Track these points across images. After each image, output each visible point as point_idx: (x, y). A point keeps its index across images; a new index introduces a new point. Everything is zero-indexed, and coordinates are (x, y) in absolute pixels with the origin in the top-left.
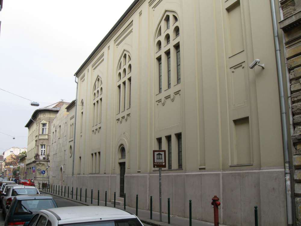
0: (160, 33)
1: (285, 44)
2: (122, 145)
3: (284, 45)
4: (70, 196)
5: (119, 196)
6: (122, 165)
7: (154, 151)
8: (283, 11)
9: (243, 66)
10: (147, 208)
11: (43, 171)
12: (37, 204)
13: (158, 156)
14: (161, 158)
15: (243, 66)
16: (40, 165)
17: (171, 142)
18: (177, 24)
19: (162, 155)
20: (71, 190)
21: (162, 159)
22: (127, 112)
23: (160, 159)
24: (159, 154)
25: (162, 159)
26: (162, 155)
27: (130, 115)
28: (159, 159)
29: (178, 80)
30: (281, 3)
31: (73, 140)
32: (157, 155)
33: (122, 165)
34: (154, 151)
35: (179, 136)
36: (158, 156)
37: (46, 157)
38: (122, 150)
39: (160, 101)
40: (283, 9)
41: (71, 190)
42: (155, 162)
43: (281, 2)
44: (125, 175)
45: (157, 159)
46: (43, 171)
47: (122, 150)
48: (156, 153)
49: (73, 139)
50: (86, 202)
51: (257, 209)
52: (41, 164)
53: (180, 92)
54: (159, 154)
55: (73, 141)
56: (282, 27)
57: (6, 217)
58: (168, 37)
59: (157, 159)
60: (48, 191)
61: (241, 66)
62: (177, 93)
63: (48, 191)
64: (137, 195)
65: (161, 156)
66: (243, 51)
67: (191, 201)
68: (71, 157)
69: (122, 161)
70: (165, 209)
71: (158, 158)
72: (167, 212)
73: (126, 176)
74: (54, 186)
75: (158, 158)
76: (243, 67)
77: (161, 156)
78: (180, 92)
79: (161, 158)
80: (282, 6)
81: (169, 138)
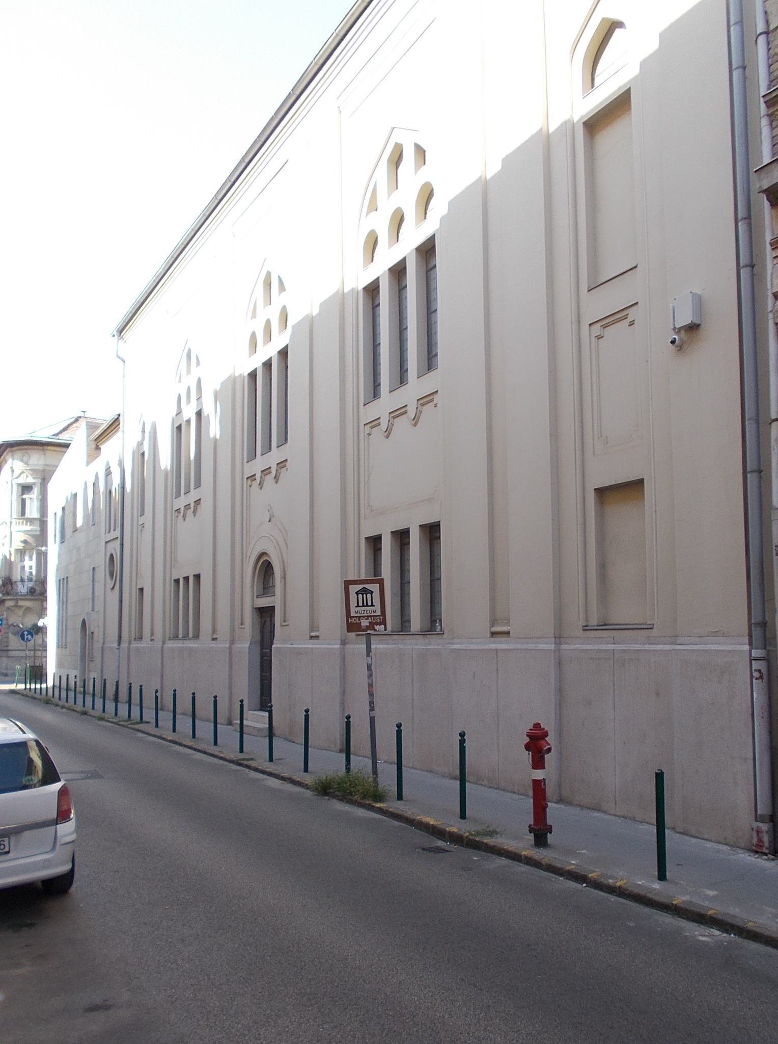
0: (373, 206)
1: (771, 244)
2: (263, 554)
3: (768, 247)
4: (110, 706)
5: (259, 707)
6: (265, 614)
7: (347, 584)
8: (772, 129)
9: (630, 319)
10: (338, 746)
11: (26, 633)
12: (73, 828)
13: (360, 596)
14: (370, 604)
15: (630, 319)
16: (20, 613)
17: (409, 548)
18: (426, 174)
19: (372, 593)
20: (184, 704)
21: (372, 605)
22: (275, 456)
23: (367, 605)
24: (364, 591)
25: (372, 605)
26: (372, 593)
27: (288, 464)
28: (363, 606)
29: (430, 360)
30: (765, 102)
31: (117, 538)
32: (357, 593)
33: (265, 614)
34: (347, 584)
35: (432, 531)
36: (360, 596)
37: (37, 588)
38: (265, 570)
39: (377, 422)
40: (775, 124)
41: (184, 704)
42: (353, 614)
43: (768, 98)
44: (273, 646)
45: (358, 606)
46: (26, 633)
47: (265, 570)
48: (353, 589)
49: (117, 533)
50: (216, 743)
51: (309, 713)
52: (20, 607)
53: (437, 398)
54: (364, 591)
55: (118, 542)
56: (765, 187)
57: (101, 493)
58: (398, 220)
59: (358, 606)
60: (71, 701)
61: (626, 317)
62: (427, 400)
63: (71, 701)
64: (194, 694)
65: (369, 595)
66: (636, 267)
67: (401, 724)
68: (113, 588)
69: (264, 602)
70: (387, 750)
71: (361, 604)
72: (369, 753)
73: (278, 649)
74: (94, 682)
75: (361, 604)
76: (632, 324)
77: (369, 595)
78: (435, 396)
79: (370, 604)
80: (771, 111)
81: (402, 537)
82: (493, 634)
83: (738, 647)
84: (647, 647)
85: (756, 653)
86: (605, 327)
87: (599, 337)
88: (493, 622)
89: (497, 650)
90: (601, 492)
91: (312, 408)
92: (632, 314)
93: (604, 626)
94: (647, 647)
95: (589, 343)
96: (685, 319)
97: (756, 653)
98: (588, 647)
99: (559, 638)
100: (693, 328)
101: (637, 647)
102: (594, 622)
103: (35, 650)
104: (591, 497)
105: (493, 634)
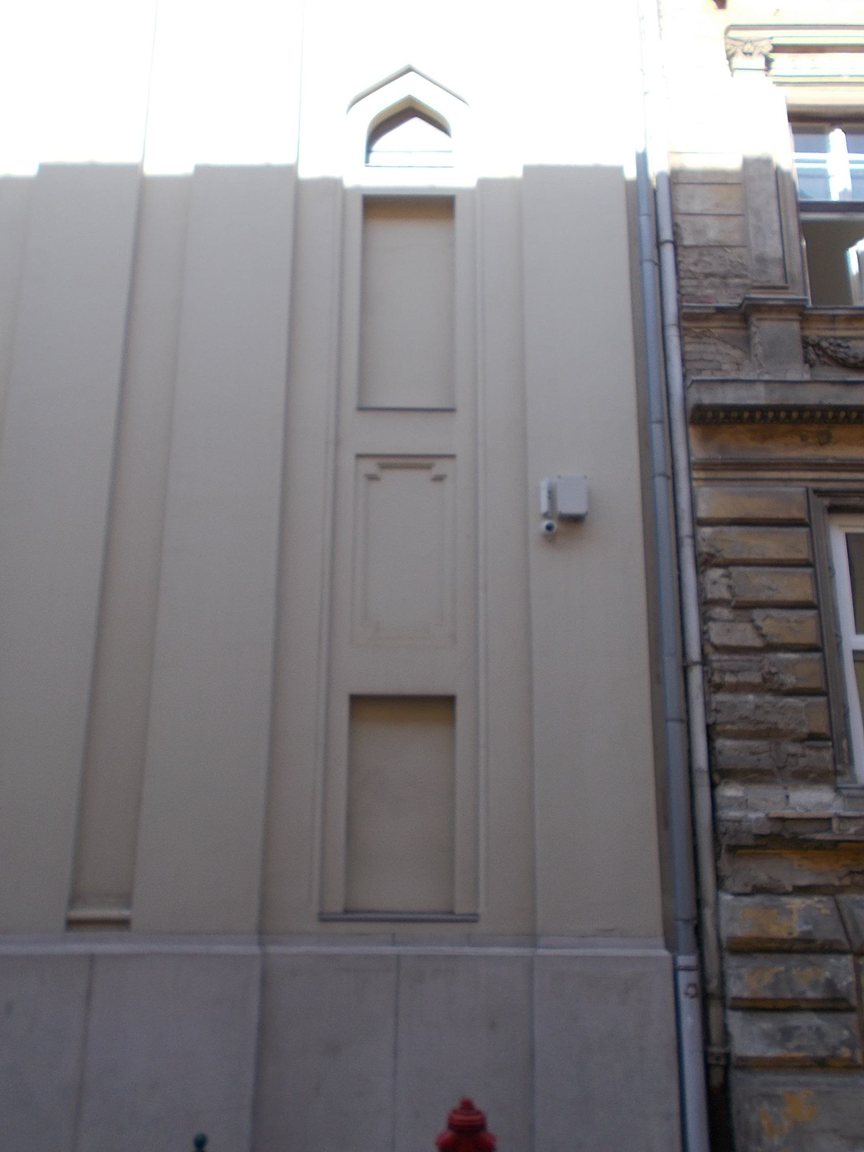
61: (428, 467)
82: (72, 924)
83: (241, 949)
84: (468, 950)
85: (683, 960)
86: (383, 467)
87: (372, 478)
88: (75, 899)
89: (92, 958)
90: (358, 702)
91: (817, 465)
92: (441, 467)
93: (350, 914)
94: (468, 950)
95: (811, 510)
96: (570, 505)
97: (683, 960)
98: (337, 950)
99: (263, 934)
100: (575, 521)
101: (448, 950)
102: (336, 905)
103: (531, 938)
104: (342, 709)
105: (72, 924)
